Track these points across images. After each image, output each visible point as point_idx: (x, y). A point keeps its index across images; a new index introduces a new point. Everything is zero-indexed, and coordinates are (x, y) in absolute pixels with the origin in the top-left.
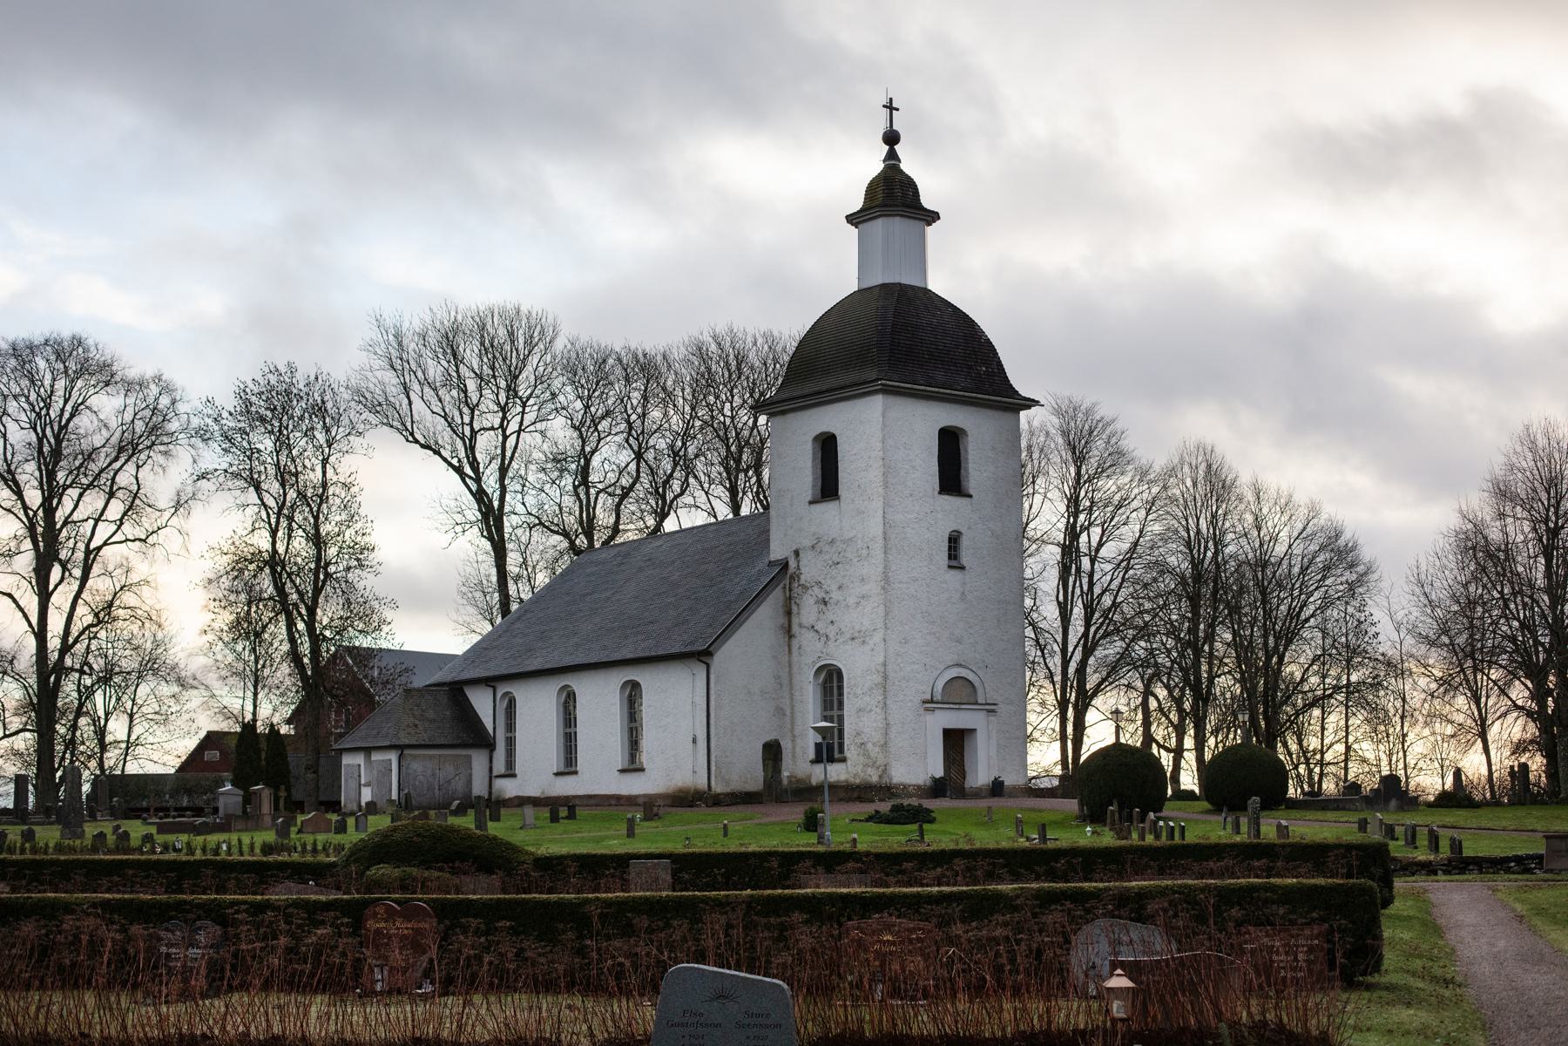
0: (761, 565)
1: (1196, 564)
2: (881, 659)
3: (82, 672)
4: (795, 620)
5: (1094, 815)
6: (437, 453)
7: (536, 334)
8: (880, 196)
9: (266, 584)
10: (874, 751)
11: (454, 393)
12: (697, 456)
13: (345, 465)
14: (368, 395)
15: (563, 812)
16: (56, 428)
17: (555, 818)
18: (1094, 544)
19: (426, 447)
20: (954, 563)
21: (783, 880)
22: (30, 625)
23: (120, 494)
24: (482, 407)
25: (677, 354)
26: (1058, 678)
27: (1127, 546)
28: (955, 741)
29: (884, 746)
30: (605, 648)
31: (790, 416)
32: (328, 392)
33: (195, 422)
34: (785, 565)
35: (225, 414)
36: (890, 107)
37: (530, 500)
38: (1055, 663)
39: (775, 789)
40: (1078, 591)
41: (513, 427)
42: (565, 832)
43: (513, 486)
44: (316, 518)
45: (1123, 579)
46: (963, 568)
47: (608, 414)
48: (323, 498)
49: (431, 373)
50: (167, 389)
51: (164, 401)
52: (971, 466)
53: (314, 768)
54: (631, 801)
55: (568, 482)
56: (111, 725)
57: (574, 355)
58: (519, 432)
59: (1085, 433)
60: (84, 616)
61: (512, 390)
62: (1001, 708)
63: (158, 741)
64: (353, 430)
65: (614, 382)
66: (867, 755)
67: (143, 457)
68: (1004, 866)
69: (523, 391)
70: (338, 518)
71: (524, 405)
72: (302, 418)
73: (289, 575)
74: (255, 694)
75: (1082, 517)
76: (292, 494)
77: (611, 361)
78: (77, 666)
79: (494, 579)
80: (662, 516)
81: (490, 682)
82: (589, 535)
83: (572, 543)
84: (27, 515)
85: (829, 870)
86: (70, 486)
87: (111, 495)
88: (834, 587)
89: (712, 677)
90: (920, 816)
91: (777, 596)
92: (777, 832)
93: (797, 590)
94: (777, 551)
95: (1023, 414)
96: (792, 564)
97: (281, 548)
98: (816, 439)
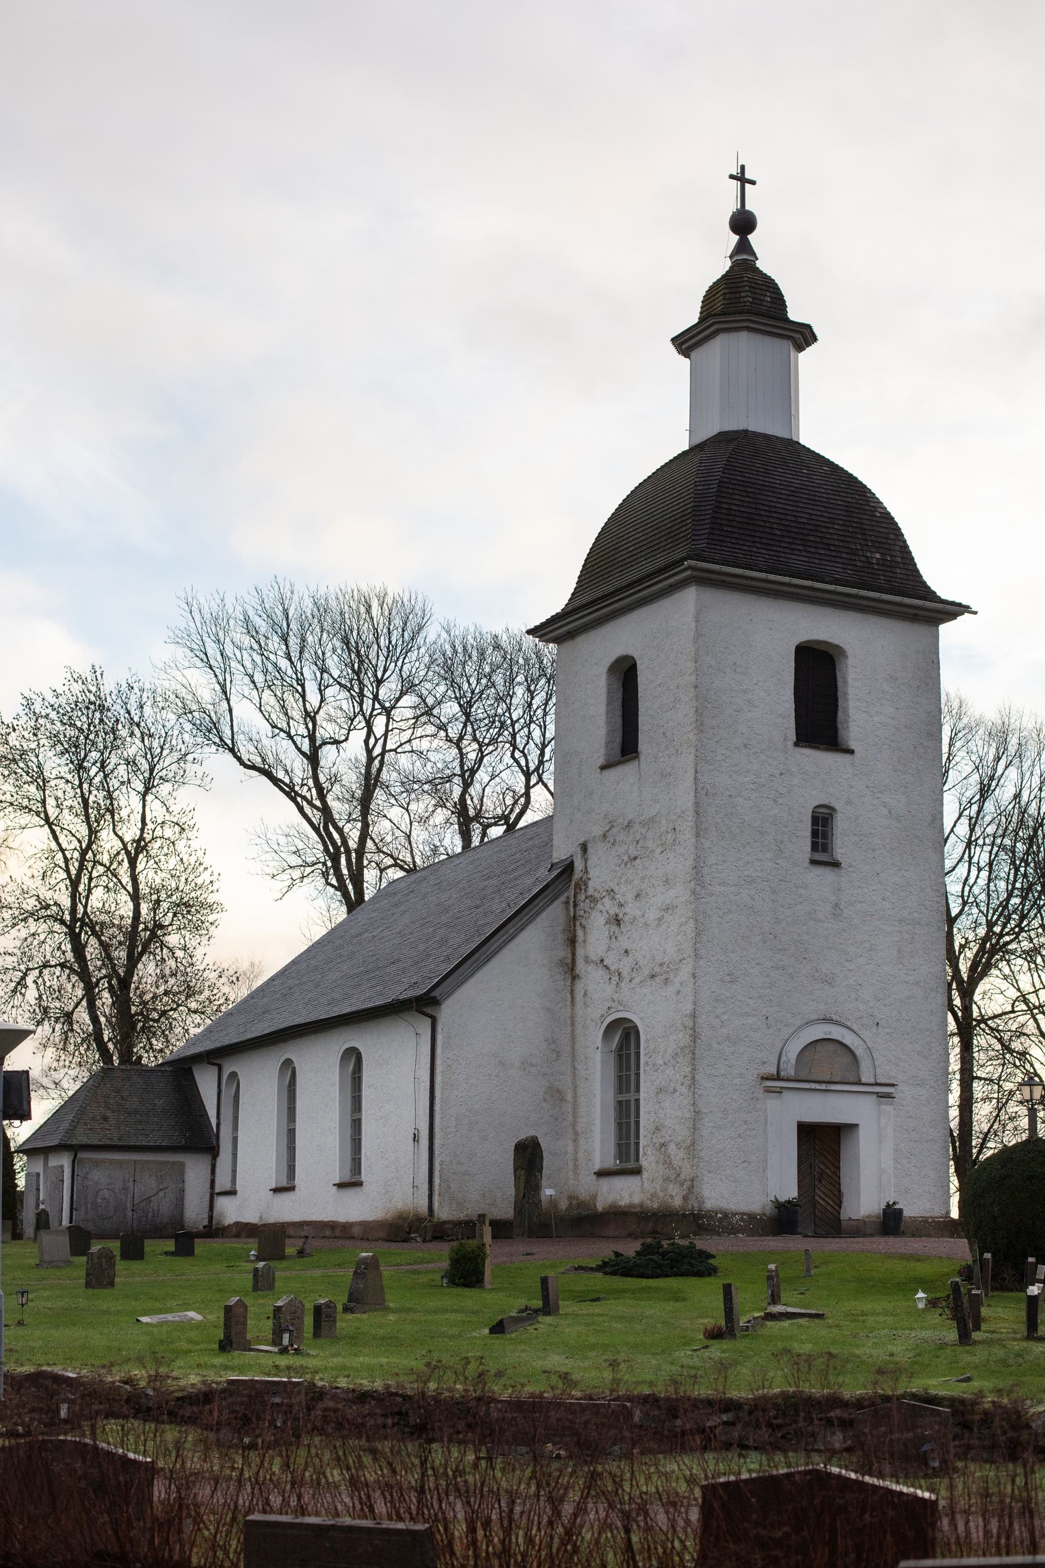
2: (689, 1008)
4: (580, 952)
7: (409, 623)
20: (820, 857)
29: (692, 1148)
34: (569, 868)
36: (741, 178)
46: (836, 865)
52: (852, 704)
62: (904, 1092)
66: (668, 1163)
88: (630, 896)
89: (439, 1038)
91: (553, 915)
96: (579, 865)
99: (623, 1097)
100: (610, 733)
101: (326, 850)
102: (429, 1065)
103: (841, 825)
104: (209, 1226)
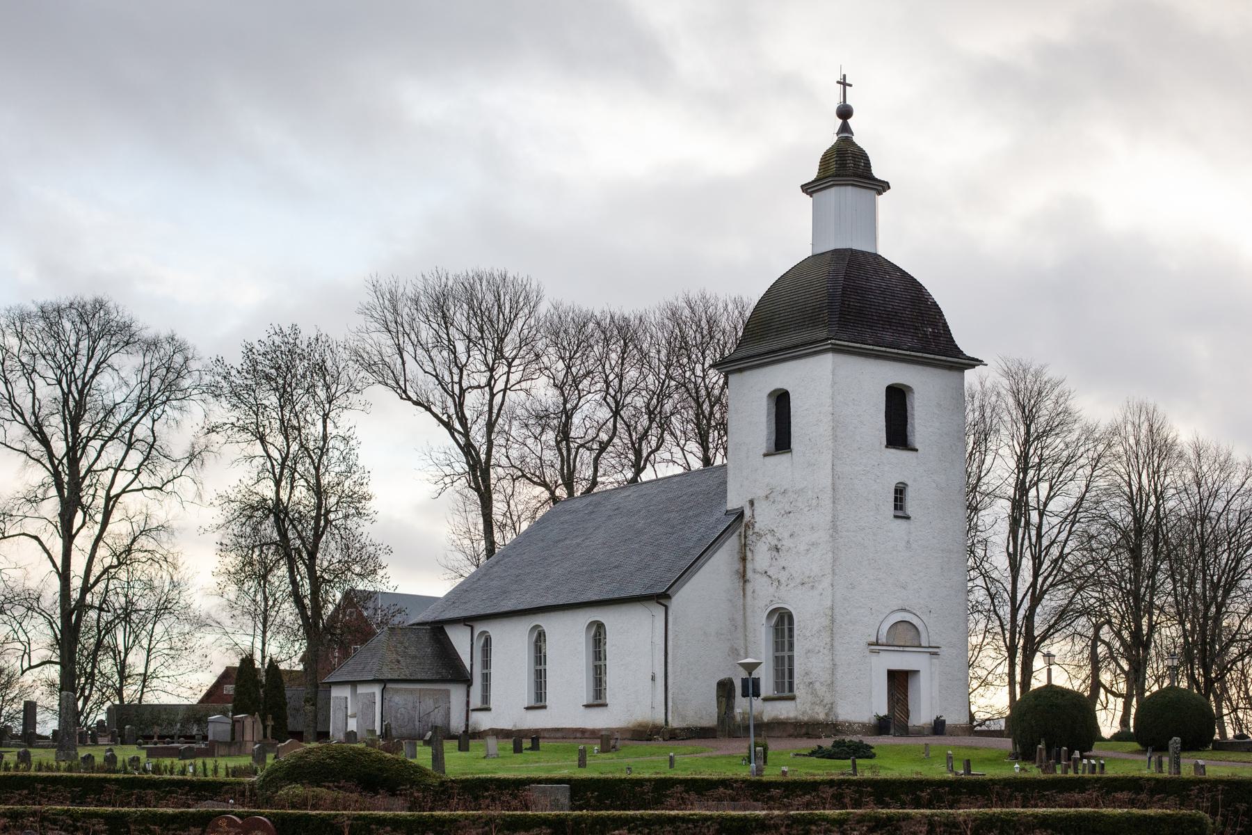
0: (719, 514)
1: (1138, 519)
2: (829, 603)
3: (101, 609)
4: (749, 566)
5: (1025, 754)
6: (428, 409)
7: (524, 299)
8: (833, 167)
9: (269, 529)
10: (821, 690)
11: (445, 353)
12: (672, 414)
13: (343, 421)
14: (365, 355)
15: (527, 743)
16: (80, 383)
17: (518, 749)
18: (1043, 499)
19: (417, 403)
20: (900, 513)
21: (658, 803)
22: (55, 565)
23: (139, 445)
24: (471, 367)
25: (654, 318)
26: (1008, 627)
27: (1073, 501)
28: (899, 681)
30: (573, 591)
31: (747, 374)
32: (328, 352)
33: (207, 379)
35: (234, 372)
36: (844, 83)
37: (514, 453)
38: (1005, 611)
39: (727, 727)
40: (1026, 543)
41: (500, 385)
42: (526, 762)
43: (499, 440)
44: (317, 469)
45: (1070, 533)
46: (908, 518)
47: (588, 373)
48: (323, 451)
49: (423, 335)
50: (180, 348)
51: (178, 359)
53: (313, 701)
54: (593, 734)
55: (550, 436)
56: (131, 659)
57: (556, 319)
58: (505, 391)
59: (1035, 394)
60: (104, 556)
61: (499, 352)
62: (944, 651)
63: (180, 677)
64: (352, 388)
65: (592, 343)
66: (814, 693)
67: (159, 411)
68: (870, 794)
69: (508, 351)
70: (337, 469)
71: (510, 366)
72: (304, 376)
73: (291, 521)
74: (264, 632)
75: (1031, 473)
76: (295, 447)
77: (591, 325)
78: (97, 604)
79: (481, 527)
80: (639, 470)
81: (468, 621)
82: (569, 484)
83: (552, 493)
84: (52, 463)
85: (700, 794)
86: (93, 438)
87: (130, 446)
88: (786, 535)
90: (862, 751)
91: (732, 543)
92: (724, 762)
93: (751, 538)
94: (734, 501)
95: (968, 374)
96: (748, 513)
97: (284, 498)
98: (770, 395)
99: (780, 654)
100: (769, 434)
101: (468, 463)
102: (489, 611)
103: (910, 495)
104: (466, 732)
